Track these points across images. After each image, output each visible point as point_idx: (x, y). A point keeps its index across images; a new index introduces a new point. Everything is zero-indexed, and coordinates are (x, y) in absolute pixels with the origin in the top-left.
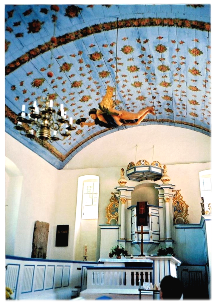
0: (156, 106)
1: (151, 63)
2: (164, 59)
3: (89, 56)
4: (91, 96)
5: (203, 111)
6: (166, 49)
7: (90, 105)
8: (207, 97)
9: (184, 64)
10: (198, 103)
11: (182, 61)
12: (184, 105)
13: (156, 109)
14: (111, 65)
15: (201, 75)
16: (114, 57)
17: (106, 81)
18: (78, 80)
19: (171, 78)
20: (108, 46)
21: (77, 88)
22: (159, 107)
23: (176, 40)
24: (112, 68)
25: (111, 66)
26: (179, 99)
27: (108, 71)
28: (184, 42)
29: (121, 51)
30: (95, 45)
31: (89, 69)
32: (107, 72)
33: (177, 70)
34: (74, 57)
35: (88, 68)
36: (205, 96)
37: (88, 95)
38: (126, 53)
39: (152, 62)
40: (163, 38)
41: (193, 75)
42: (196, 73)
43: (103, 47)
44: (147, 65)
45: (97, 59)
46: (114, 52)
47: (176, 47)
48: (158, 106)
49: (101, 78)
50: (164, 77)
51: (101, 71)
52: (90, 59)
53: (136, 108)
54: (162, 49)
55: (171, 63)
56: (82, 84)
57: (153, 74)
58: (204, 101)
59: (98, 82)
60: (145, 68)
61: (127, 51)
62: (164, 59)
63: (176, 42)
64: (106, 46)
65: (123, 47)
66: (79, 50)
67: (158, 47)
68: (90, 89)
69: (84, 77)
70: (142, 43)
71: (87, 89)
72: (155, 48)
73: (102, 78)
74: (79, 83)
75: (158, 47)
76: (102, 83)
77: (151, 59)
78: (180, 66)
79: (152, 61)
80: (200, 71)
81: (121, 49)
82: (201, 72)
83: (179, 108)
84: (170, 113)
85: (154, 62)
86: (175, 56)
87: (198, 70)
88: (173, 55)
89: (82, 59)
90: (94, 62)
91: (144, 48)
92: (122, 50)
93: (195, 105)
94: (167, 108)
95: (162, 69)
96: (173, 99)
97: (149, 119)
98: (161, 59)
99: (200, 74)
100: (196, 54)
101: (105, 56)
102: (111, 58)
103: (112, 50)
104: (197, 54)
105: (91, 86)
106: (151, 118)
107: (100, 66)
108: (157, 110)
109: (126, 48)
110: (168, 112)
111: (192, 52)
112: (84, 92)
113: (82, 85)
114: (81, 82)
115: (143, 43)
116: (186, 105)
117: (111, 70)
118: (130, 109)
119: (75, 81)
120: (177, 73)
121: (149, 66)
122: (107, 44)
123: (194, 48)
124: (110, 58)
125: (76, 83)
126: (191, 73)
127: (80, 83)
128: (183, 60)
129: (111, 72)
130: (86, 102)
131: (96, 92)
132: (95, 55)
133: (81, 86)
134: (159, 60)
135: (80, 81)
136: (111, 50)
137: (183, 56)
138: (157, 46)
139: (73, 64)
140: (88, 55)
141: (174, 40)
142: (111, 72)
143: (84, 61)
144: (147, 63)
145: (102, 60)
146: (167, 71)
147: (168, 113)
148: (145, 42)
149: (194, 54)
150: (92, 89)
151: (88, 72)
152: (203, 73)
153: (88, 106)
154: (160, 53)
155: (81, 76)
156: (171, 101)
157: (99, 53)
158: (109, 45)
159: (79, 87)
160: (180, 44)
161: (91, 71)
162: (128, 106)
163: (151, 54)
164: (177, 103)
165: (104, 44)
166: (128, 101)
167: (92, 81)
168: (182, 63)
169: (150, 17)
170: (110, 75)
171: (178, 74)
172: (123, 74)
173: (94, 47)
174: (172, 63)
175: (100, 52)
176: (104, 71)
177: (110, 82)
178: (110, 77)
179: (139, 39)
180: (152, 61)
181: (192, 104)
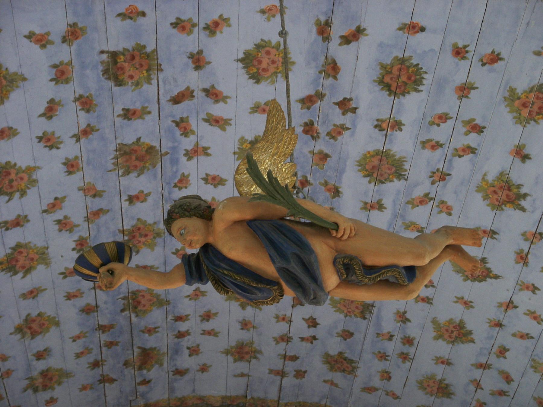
0: (296, 339)
1: (339, 138)
2: (398, 125)
3: (105, 57)
4: (52, 252)
5: (477, 374)
6: (418, 82)
7: (31, 292)
8: (516, 307)
9: (471, 155)
10: (470, 333)
11: (466, 143)
12: (408, 341)
13: (292, 354)
14: (178, 119)
15: (523, 209)
16: (201, 87)
17: (133, 193)
18: (23, 162)
19: (395, 216)
20: (196, 29)
21: (7, 198)
22: (304, 344)
23: (471, 48)
24: (178, 132)
25: (177, 124)
26: (398, 312)
27: (158, 148)
28: (501, 59)
29: (240, 65)
30: (146, 11)
31: (84, 119)
32: (151, 149)
33: (433, 183)
34: (43, 46)
35: (82, 114)
36: (511, 302)
37: (40, 244)
38: (256, 78)
39: (346, 133)
40: (423, 29)
41: (489, 208)
42: (504, 197)
43: (175, 31)
44: (321, 146)
45: (131, 77)
46: (209, 63)
47: (460, 79)
48: (302, 339)
49: (121, 172)
50: (372, 207)
51: (129, 139)
52: (106, 72)
53: (211, 337)
54: (403, 78)
55: (419, 146)
56: (34, 182)
57: (329, 190)
58: (499, 325)
59: (99, 187)
60: (310, 156)
61: (264, 70)
62: (398, 125)
63: (469, 55)
64: (188, 26)
65: (250, 46)
66: (71, 21)
67: (392, 67)
68: (59, 215)
69: (54, 151)
70: (335, 41)
71: (45, 211)
72: (376, 73)
73: (124, 175)
74: (22, 179)
75: (392, 67)
76: (117, 199)
77: (347, 120)
78: (450, 161)
79: (348, 129)
80: (523, 191)
81: (241, 56)
82: (525, 196)
83: (383, 357)
84: (339, 374)
85: (353, 134)
86: (444, 118)
87: (519, 186)
88: (440, 110)
89: (70, 63)
90: (116, 89)
91: (334, 63)
92: (241, 60)
93: (453, 343)
94: (333, 352)
95: (374, 167)
96: (375, 310)
97: (249, 398)
98: (384, 125)
99: (523, 203)
100: (530, 113)
101: (168, 72)
102: (188, 88)
103: (205, 54)
104: (538, 114)
105: (66, 204)
106: (255, 395)
107: (134, 112)
108: (294, 358)
109: (263, 51)
110: (332, 369)
111: (517, 103)
112: (29, 226)
113: (32, 193)
114: (30, 176)
115: (339, 41)
116: (416, 342)
117: (170, 144)
118: (186, 342)
119: (8, 163)
120: (427, 195)
121: (326, 151)
122: (195, 21)
123: (531, 90)
124: (182, 88)
125: (8, 174)
126: (486, 197)
127: (26, 177)
128: (473, 139)
129: (167, 153)
130: (20, 275)
131: (76, 238)
132: (133, 58)
133: (23, 194)
134: (379, 127)
135: (30, 170)
136: (200, 52)
137: (478, 121)
138: (388, 61)
139: (24, 79)
140: (102, 52)
141: (465, 47)
142: (167, 153)
143: (75, 74)
144: (323, 135)
145: (150, 90)
146: (392, 181)
147: (330, 376)
148: (347, 40)
149: (525, 113)
150: (65, 217)
151: (76, 132)
152: (534, 200)
153: (24, 296)
154: (390, 95)
155: (42, 144)
156: (365, 318)
157: (148, 56)
158: (202, 25)
159: (17, 195)
160: (483, 65)
161: (87, 131)
162: (183, 327)
163: (353, 96)
164: (385, 331)
165: (183, 18)
166: (192, 303)
167: (76, 179)
168: (464, 150)
169: (144, 191)
170: (159, 165)
171: (431, 199)
172: (213, 173)
173: (141, 20)
174: (424, 148)
175: (156, 51)
176: (142, 140)
177: (150, 200)
178: (155, 177)
179: (328, 24)
180: (348, 129)
181: (444, 340)
